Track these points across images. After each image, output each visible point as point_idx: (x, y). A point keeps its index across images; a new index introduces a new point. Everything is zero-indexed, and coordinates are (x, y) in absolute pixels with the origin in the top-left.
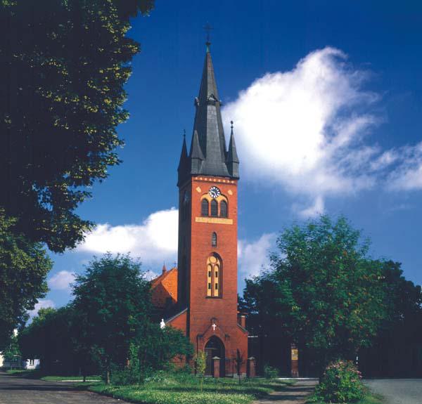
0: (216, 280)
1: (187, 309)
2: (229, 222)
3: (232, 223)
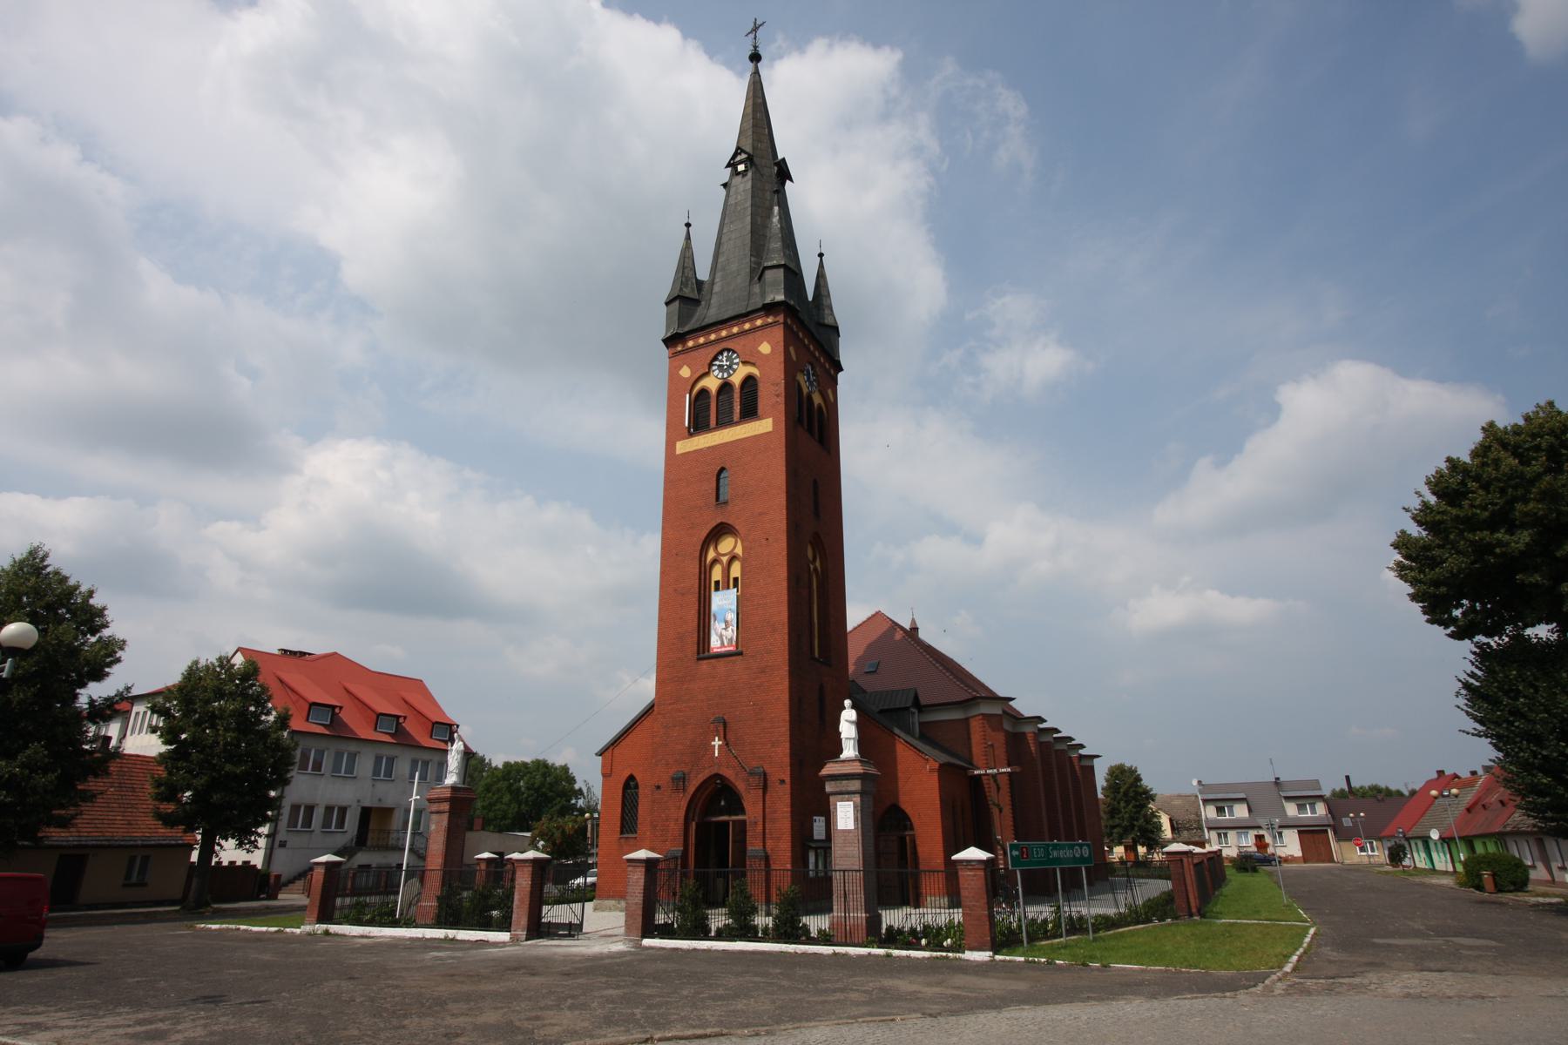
2: (763, 426)
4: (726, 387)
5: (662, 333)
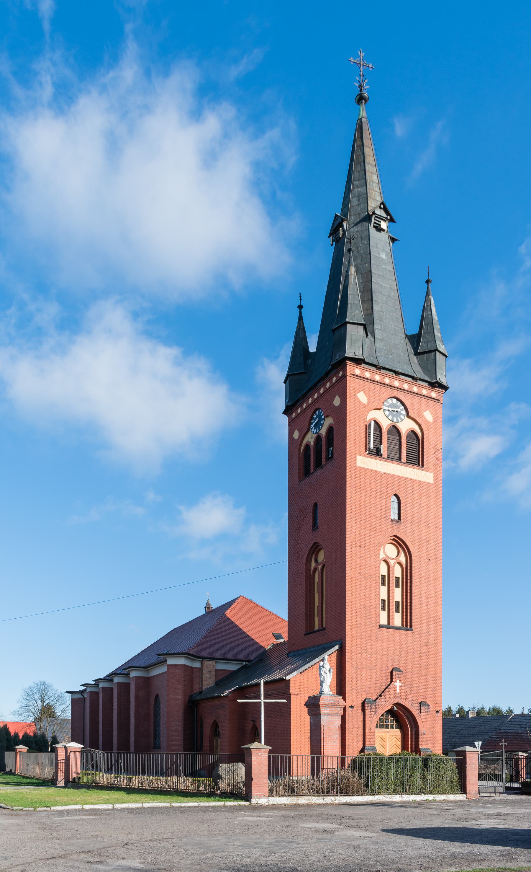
0: (397, 595)
1: (337, 647)
3: (362, 393)
4: (318, 438)
5: (283, 408)
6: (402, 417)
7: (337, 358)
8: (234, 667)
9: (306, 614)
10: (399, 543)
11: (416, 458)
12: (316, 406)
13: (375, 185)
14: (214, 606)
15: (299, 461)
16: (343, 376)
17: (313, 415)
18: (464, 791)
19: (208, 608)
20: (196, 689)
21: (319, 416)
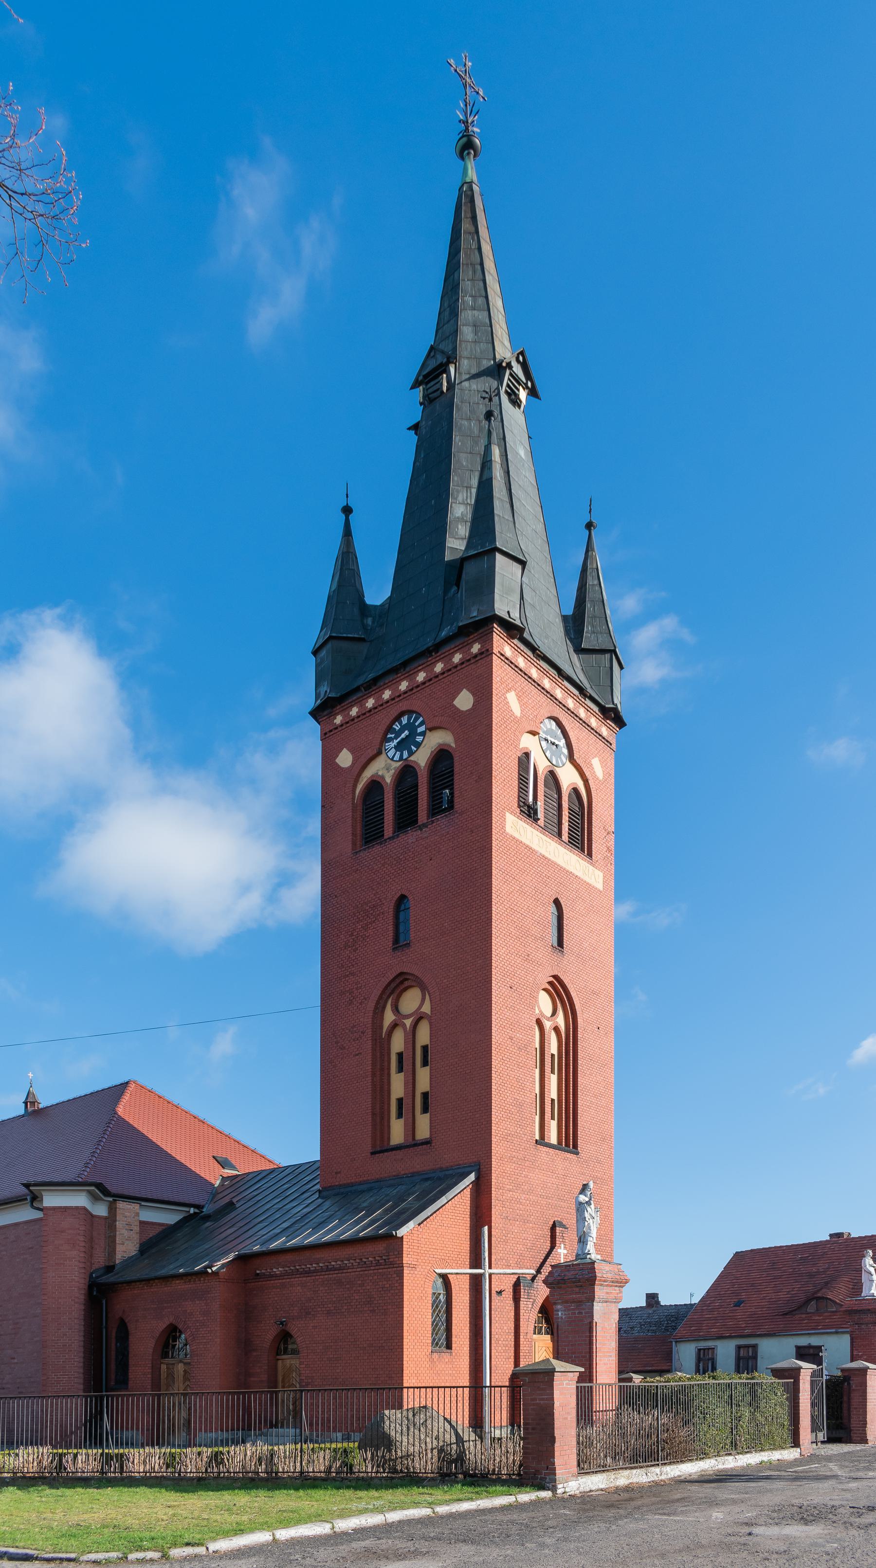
1: (472, 1177)
4: (407, 772)
5: (311, 702)
6: (419, 739)
7: (475, 614)
8: (168, 1217)
9: (374, 1114)
10: (558, 990)
11: (580, 839)
12: (404, 706)
13: (500, 316)
14: (44, 1101)
15: (354, 811)
16: (481, 653)
17: (393, 722)
18: (796, 1443)
19: (33, 1103)
20: (100, 1260)
21: (411, 727)
